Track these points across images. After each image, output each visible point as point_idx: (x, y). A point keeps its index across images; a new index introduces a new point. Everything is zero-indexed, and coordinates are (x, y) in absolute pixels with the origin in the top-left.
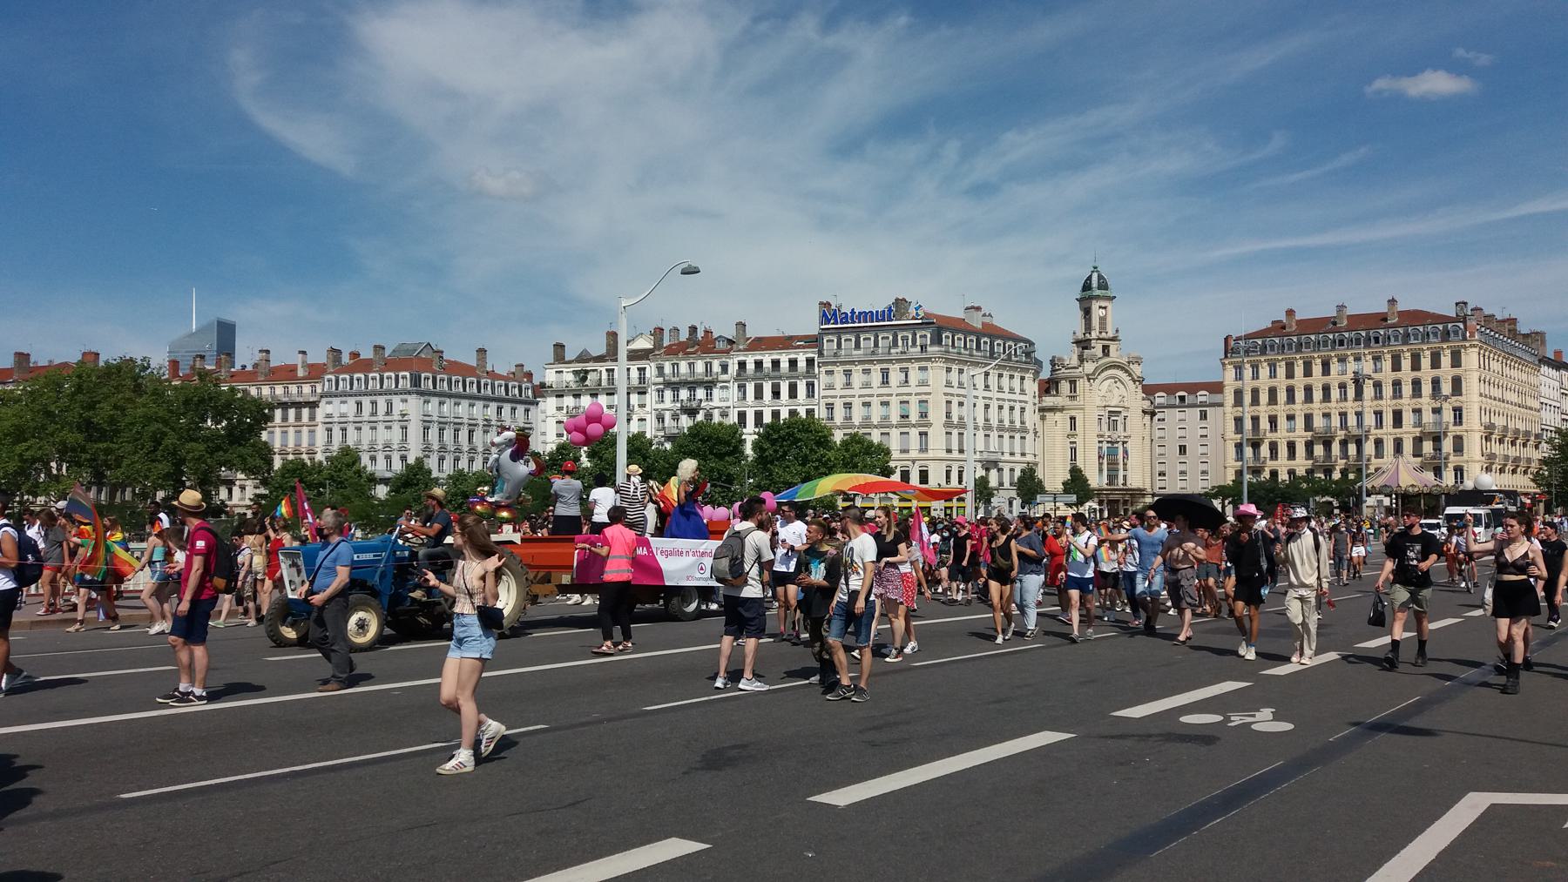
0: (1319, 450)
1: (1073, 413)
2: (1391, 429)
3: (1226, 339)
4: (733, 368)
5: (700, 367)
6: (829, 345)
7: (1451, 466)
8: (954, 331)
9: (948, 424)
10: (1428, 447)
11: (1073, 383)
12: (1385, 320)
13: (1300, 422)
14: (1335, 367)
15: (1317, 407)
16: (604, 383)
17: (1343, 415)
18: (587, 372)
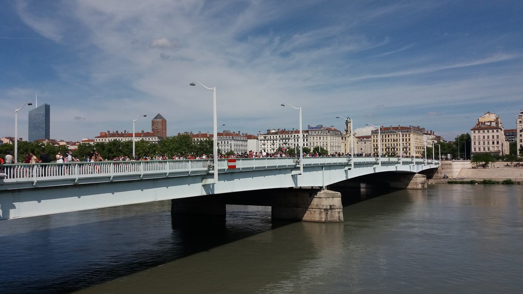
0: (387, 150)
1: (346, 143)
2: (399, 147)
3: (372, 131)
4: (293, 136)
5: (287, 136)
6: (310, 133)
7: (408, 153)
8: (331, 131)
9: (331, 146)
10: (405, 149)
11: (345, 138)
12: (398, 128)
13: (384, 145)
14: (390, 136)
15: (387, 143)
16: (269, 139)
17: (391, 144)
18: (266, 137)
